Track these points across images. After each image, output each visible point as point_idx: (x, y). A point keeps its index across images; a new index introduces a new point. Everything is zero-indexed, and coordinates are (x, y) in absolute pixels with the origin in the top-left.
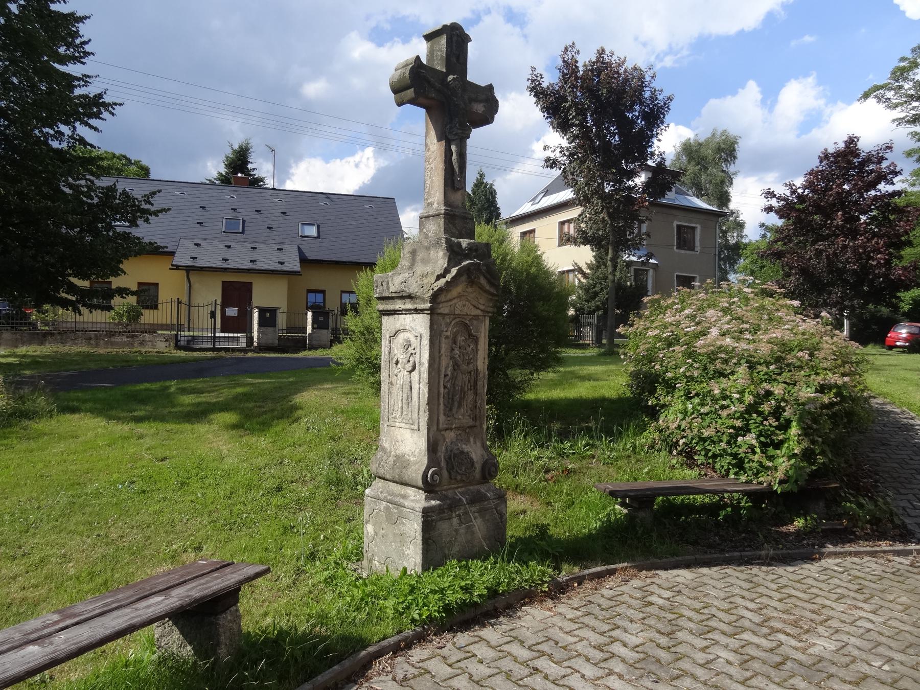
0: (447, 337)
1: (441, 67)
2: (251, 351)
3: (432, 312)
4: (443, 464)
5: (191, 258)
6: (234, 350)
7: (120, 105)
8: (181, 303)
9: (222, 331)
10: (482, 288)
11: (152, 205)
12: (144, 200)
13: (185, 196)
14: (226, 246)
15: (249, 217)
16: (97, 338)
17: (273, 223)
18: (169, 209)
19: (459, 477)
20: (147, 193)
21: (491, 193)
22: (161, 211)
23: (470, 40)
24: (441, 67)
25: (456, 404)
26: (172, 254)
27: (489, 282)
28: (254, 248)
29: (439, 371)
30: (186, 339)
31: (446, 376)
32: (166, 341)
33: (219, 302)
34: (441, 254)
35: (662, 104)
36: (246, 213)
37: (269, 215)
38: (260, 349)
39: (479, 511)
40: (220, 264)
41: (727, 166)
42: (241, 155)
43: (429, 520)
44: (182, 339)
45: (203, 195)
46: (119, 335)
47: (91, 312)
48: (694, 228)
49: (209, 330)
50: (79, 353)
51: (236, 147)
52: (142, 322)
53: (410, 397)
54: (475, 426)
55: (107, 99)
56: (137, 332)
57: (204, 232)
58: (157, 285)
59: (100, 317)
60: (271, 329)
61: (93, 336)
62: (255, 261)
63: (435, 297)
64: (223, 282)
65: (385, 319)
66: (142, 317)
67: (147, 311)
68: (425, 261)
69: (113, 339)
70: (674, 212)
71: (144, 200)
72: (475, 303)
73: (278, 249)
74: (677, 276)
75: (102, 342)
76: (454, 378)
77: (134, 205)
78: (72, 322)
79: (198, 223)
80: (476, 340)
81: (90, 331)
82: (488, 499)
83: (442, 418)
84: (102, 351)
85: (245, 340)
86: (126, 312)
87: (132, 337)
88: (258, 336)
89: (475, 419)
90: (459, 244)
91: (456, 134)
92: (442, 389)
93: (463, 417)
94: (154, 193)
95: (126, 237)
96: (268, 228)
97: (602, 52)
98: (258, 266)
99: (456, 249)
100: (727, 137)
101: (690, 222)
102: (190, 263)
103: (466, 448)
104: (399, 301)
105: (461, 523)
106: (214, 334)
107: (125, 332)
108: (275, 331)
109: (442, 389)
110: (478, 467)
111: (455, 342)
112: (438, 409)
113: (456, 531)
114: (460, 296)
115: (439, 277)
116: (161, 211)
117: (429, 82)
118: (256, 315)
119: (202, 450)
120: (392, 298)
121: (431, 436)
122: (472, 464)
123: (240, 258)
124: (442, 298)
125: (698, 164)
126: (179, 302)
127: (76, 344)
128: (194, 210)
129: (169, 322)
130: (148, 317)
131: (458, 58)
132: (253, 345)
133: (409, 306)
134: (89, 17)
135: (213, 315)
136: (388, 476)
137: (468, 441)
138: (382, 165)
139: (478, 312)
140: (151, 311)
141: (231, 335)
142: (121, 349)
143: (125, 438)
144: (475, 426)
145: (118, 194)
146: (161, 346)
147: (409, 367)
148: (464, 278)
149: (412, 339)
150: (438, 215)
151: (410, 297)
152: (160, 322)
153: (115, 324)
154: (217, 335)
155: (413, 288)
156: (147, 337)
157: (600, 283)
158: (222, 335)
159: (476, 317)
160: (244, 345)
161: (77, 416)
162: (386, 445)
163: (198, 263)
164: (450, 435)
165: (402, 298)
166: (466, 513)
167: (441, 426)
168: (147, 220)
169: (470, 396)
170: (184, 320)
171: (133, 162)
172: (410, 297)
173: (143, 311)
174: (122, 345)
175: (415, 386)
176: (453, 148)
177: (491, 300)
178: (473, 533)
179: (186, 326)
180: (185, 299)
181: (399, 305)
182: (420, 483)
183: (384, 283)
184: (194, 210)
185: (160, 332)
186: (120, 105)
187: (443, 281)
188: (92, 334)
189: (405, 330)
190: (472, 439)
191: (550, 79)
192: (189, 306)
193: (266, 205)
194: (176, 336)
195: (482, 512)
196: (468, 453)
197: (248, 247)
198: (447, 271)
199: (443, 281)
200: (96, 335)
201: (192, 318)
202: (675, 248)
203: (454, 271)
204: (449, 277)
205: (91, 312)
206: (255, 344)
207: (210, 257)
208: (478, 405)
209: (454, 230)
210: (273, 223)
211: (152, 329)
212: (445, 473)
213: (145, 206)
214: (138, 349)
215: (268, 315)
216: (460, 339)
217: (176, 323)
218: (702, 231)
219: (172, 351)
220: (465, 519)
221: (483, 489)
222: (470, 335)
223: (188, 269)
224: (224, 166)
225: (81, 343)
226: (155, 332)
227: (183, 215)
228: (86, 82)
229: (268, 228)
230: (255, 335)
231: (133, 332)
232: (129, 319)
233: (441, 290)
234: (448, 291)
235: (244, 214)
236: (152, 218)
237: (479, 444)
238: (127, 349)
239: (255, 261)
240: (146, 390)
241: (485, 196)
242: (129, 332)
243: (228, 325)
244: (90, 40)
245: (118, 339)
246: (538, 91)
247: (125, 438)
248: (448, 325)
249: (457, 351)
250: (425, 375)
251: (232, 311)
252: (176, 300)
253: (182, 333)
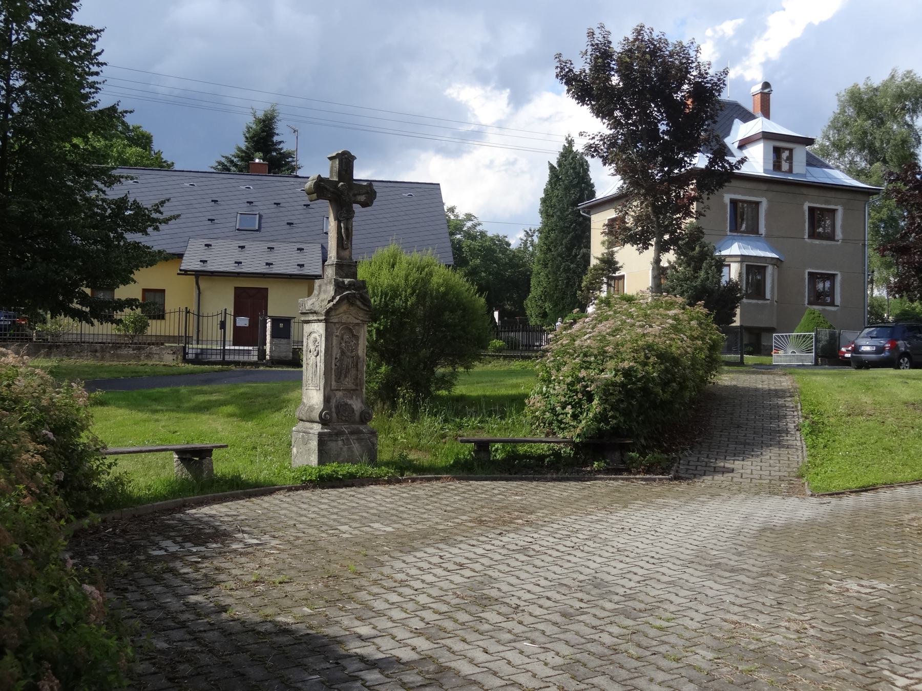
0: (337, 336)
1: (335, 179)
2: (263, 365)
3: (326, 321)
4: (333, 410)
5: (201, 261)
6: (244, 364)
7: (131, 112)
8: (189, 312)
9: (234, 345)
10: (359, 307)
11: (161, 213)
12: (154, 210)
13: (195, 188)
14: (239, 247)
15: (267, 211)
16: (103, 350)
17: (293, 217)
18: (179, 216)
19: (344, 418)
20: (157, 202)
21: (582, 165)
22: (170, 219)
23: (354, 158)
24: (335, 179)
25: (343, 376)
26: (180, 256)
27: (363, 303)
28: (271, 248)
29: (331, 355)
30: (194, 351)
31: (336, 358)
32: (174, 353)
33: (231, 310)
34: (332, 288)
35: (715, 80)
36: (264, 207)
37: (289, 209)
38: (273, 363)
39: (357, 440)
40: (232, 268)
41: (912, 119)
42: (265, 126)
43: (322, 440)
44: (190, 351)
45: (214, 187)
46: (125, 347)
47: (102, 324)
48: (834, 211)
49: (219, 342)
50: (87, 366)
51: (260, 115)
52: (149, 333)
53: (316, 371)
54: (357, 390)
55: (120, 109)
56: (145, 344)
57: (216, 231)
58: (163, 291)
59: (103, 330)
60: (284, 341)
61: (98, 348)
62: (272, 264)
63: (328, 313)
64: (236, 288)
65: (305, 325)
66: (149, 328)
67: (154, 321)
68: (325, 292)
69: (119, 352)
70: (805, 191)
71: (154, 210)
72: (355, 316)
73: (298, 249)
74: (809, 273)
75: (108, 355)
76: (341, 360)
77: (145, 215)
78: (77, 334)
79: (209, 220)
80: (357, 338)
81: (96, 343)
82: (364, 433)
83: (334, 383)
84: (107, 364)
85: (256, 353)
86: (132, 322)
87: (139, 349)
88: (271, 348)
89: (357, 385)
90: (343, 282)
92: (333, 366)
93: (348, 383)
94: (163, 203)
95: (136, 246)
96: (288, 224)
97: (639, 31)
98: (276, 270)
99: (341, 285)
100: (912, 80)
101: (827, 202)
102: (198, 266)
103: (349, 402)
104: (311, 315)
105: (344, 445)
106: (224, 347)
107: (131, 344)
108: (289, 344)
109: (333, 366)
110: (357, 414)
111: (342, 339)
112: (331, 378)
113: (341, 449)
114: (345, 312)
115: (329, 302)
116: (170, 219)
117: (326, 189)
118: (269, 325)
119: (204, 428)
120: (307, 313)
121: (326, 392)
122: (353, 411)
123: (254, 262)
124: (333, 313)
125: (870, 117)
126: (188, 312)
127: (82, 357)
128: (205, 205)
129: (176, 334)
130: (155, 328)
131: (346, 171)
132: (265, 358)
133: (315, 318)
134: (103, 30)
135: (223, 325)
136: (304, 419)
137: (352, 398)
139: (358, 321)
140: (159, 321)
141: (242, 348)
142: (127, 363)
143: (145, 421)
144: (357, 390)
145: (130, 204)
146: (169, 359)
147: (315, 354)
148: (345, 301)
149: (318, 337)
150: (332, 265)
151: (315, 313)
152: (167, 334)
153: (120, 336)
154: (226, 348)
155: (317, 308)
156: (154, 348)
157: (681, 286)
158: (232, 348)
159: (358, 324)
160: (255, 359)
161: (106, 408)
162: (305, 401)
163: (210, 267)
164: (339, 394)
165: (312, 313)
166: (348, 439)
167: (333, 388)
168: (157, 229)
169: (353, 372)
170: (192, 332)
171: (131, 128)
172: (315, 313)
173: (150, 321)
174: (128, 358)
175: (318, 364)
176: (342, 225)
177: (367, 314)
178: (352, 452)
179: (195, 338)
180: (193, 309)
181: (311, 317)
182: (318, 419)
183: (303, 304)
184: (205, 205)
185: (167, 345)
186: (131, 112)
187: (332, 303)
188: (98, 347)
189: (314, 332)
190: (354, 397)
191: (581, 66)
192: (198, 316)
193: (286, 196)
194: (184, 348)
195: (359, 440)
196: (350, 405)
197: (264, 246)
198: (334, 298)
199: (332, 303)
200: (102, 347)
201: (200, 329)
202: (806, 236)
203: (338, 298)
204: (335, 301)
205: (102, 324)
206: (268, 357)
207: (222, 260)
208: (359, 377)
210: (293, 217)
211: (160, 341)
212: (334, 415)
213: (155, 215)
214: (145, 362)
215: (281, 325)
216: (346, 337)
217: (183, 335)
218: (844, 215)
219: (180, 364)
220: (347, 442)
221: (361, 428)
222: (354, 336)
223: (198, 275)
224: (244, 139)
225: (87, 356)
226: (162, 344)
227: (193, 211)
228: (97, 88)
229: (288, 224)
230: (268, 347)
231: (140, 344)
232: (136, 330)
233: (330, 308)
234: (336, 309)
235: (262, 207)
236: (162, 227)
237: (359, 400)
238: (133, 362)
239: (272, 264)
240: (158, 392)
241: (574, 168)
242: (136, 344)
243: (241, 337)
244: (103, 51)
245: (124, 352)
246: (570, 79)
247: (145, 421)
248: (337, 329)
249: (343, 344)
250: (323, 358)
251: (243, 322)
252: (184, 310)
253: (190, 346)
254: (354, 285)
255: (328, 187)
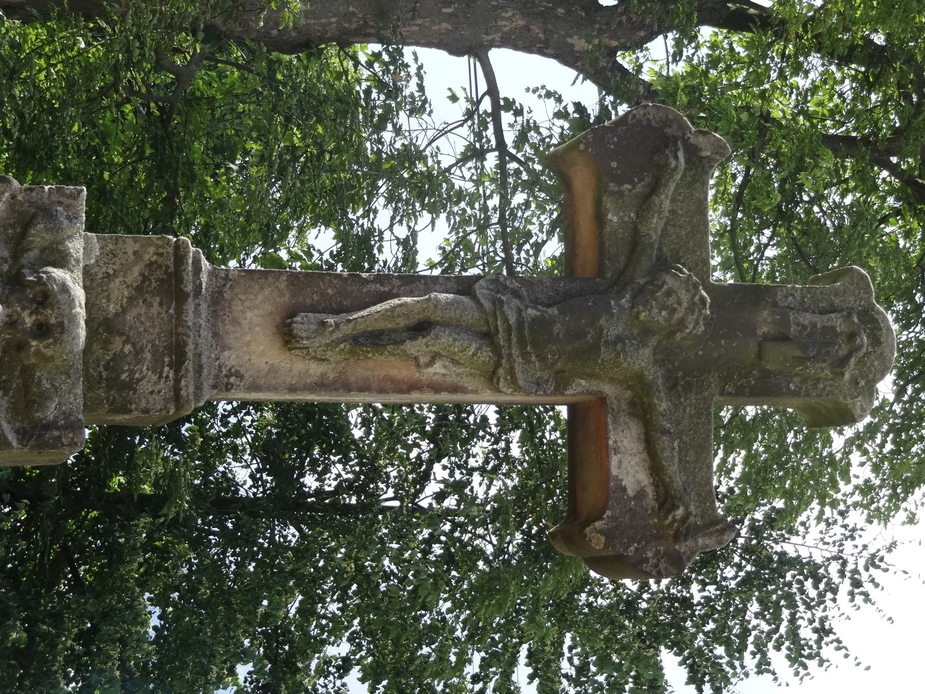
91: (498, 303)
99: (39, 235)
117: (655, 188)
138: (268, 307)
209: (119, 290)
254: (42, 330)
255: (665, 201)
